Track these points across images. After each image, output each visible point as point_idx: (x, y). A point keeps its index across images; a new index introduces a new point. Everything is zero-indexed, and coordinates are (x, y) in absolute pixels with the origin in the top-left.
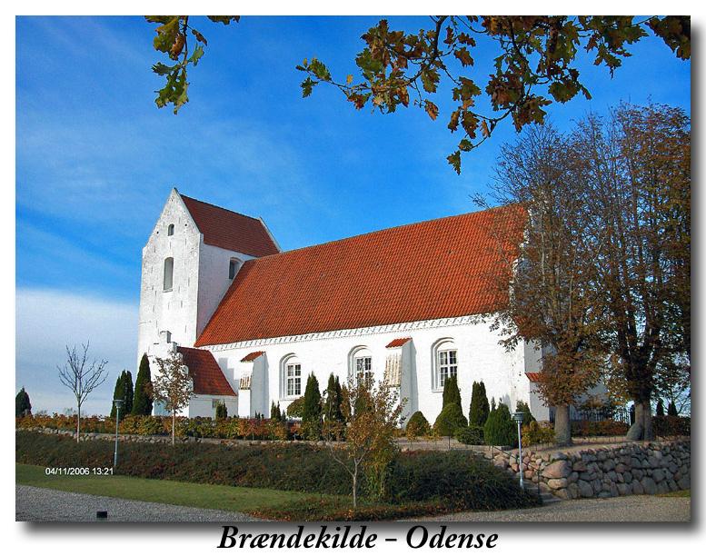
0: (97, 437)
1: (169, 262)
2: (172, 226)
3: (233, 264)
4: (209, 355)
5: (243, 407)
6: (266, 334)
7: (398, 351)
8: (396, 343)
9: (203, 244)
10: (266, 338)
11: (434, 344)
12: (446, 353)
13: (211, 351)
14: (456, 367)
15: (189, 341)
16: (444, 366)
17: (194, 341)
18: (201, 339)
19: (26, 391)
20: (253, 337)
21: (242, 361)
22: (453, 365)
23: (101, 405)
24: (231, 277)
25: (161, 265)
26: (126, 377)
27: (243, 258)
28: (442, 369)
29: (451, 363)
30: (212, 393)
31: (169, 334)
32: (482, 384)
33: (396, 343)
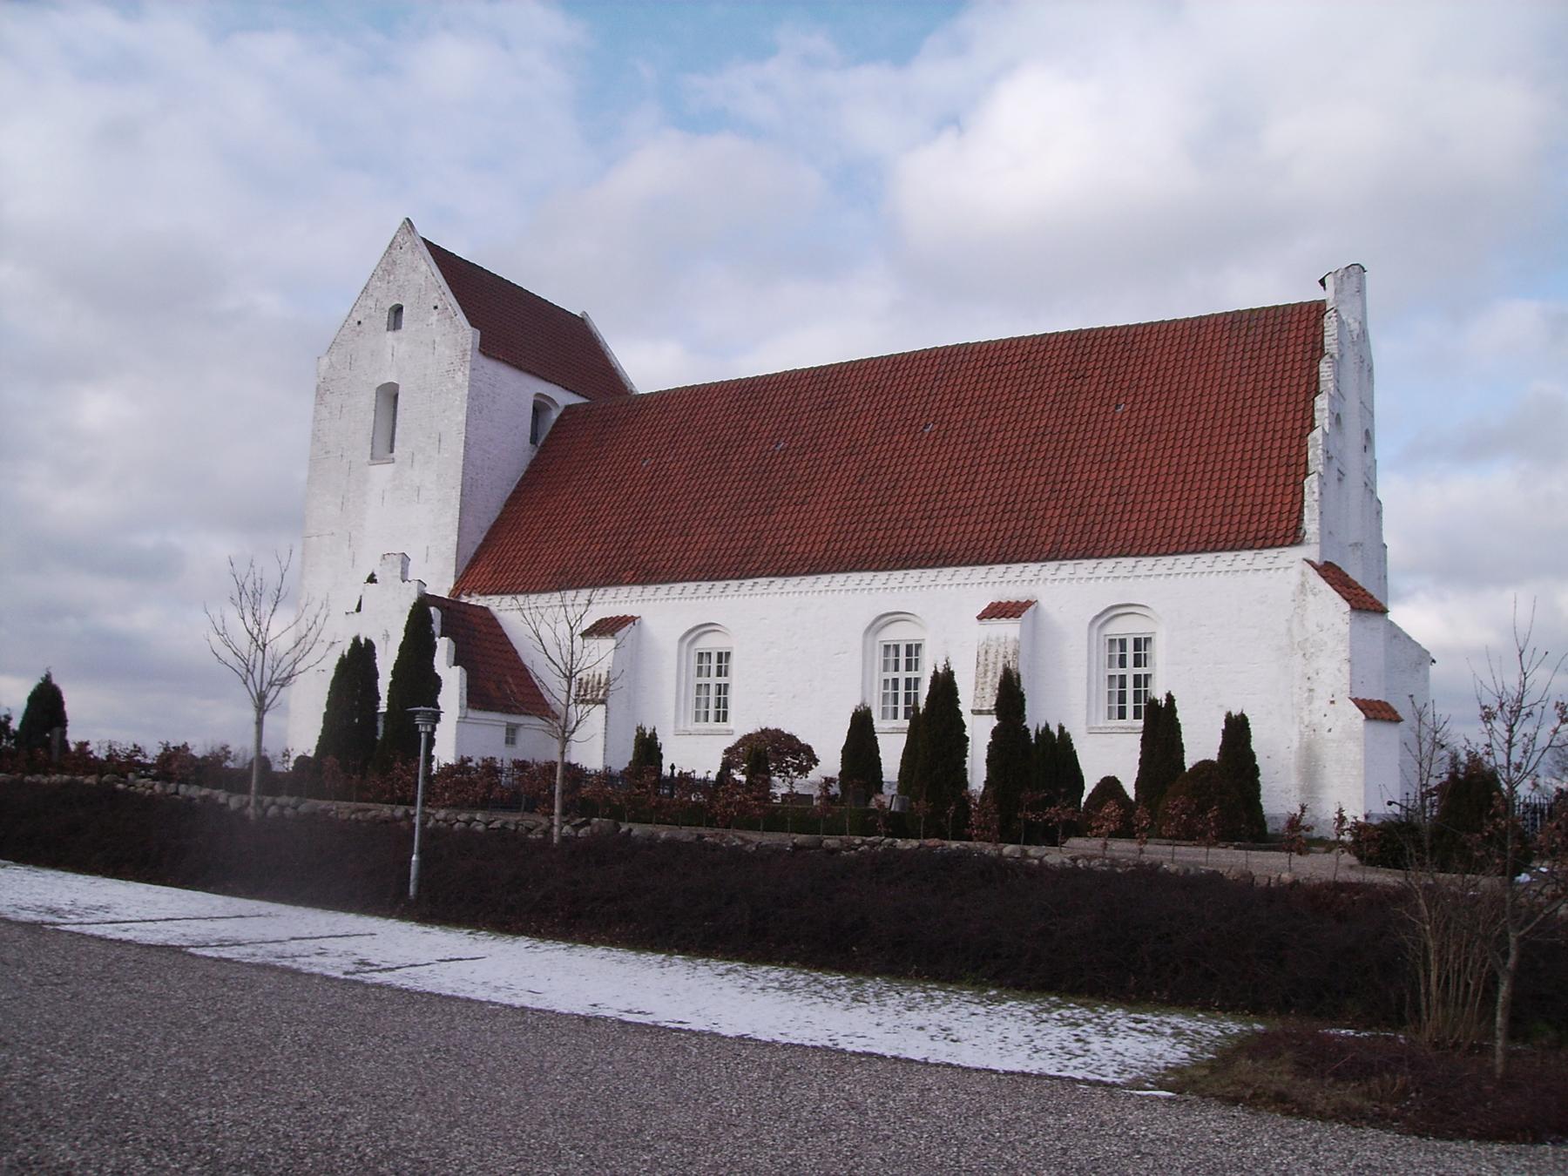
0: (303, 808)
1: (390, 395)
2: (398, 310)
3: (540, 408)
4: (488, 620)
5: (594, 746)
6: (647, 574)
7: (1008, 629)
8: (998, 611)
9: (477, 353)
10: (643, 583)
11: (1098, 617)
12: (897, 647)
13: (493, 609)
14: (917, 680)
15: (441, 586)
16: (1118, 671)
17: (451, 584)
18: (465, 581)
19: (55, 681)
20: (611, 578)
21: (980, 618)
22: (723, 680)
23: (300, 728)
24: (534, 440)
25: (366, 403)
26: (360, 658)
27: (563, 398)
28: (699, 686)
29: (908, 668)
30: (507, 709)
31: (405, 559)
32: (1243, 716)
33: (998, 611)
